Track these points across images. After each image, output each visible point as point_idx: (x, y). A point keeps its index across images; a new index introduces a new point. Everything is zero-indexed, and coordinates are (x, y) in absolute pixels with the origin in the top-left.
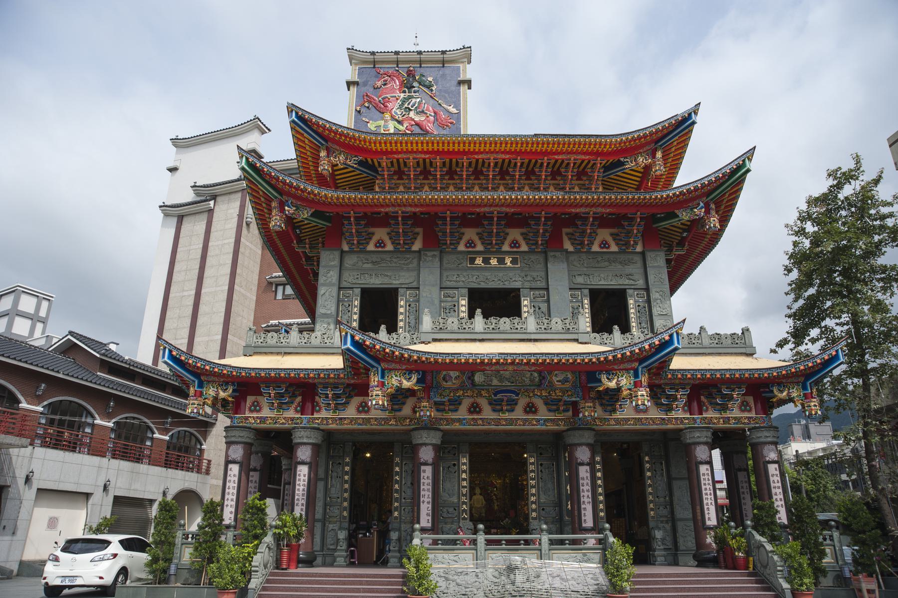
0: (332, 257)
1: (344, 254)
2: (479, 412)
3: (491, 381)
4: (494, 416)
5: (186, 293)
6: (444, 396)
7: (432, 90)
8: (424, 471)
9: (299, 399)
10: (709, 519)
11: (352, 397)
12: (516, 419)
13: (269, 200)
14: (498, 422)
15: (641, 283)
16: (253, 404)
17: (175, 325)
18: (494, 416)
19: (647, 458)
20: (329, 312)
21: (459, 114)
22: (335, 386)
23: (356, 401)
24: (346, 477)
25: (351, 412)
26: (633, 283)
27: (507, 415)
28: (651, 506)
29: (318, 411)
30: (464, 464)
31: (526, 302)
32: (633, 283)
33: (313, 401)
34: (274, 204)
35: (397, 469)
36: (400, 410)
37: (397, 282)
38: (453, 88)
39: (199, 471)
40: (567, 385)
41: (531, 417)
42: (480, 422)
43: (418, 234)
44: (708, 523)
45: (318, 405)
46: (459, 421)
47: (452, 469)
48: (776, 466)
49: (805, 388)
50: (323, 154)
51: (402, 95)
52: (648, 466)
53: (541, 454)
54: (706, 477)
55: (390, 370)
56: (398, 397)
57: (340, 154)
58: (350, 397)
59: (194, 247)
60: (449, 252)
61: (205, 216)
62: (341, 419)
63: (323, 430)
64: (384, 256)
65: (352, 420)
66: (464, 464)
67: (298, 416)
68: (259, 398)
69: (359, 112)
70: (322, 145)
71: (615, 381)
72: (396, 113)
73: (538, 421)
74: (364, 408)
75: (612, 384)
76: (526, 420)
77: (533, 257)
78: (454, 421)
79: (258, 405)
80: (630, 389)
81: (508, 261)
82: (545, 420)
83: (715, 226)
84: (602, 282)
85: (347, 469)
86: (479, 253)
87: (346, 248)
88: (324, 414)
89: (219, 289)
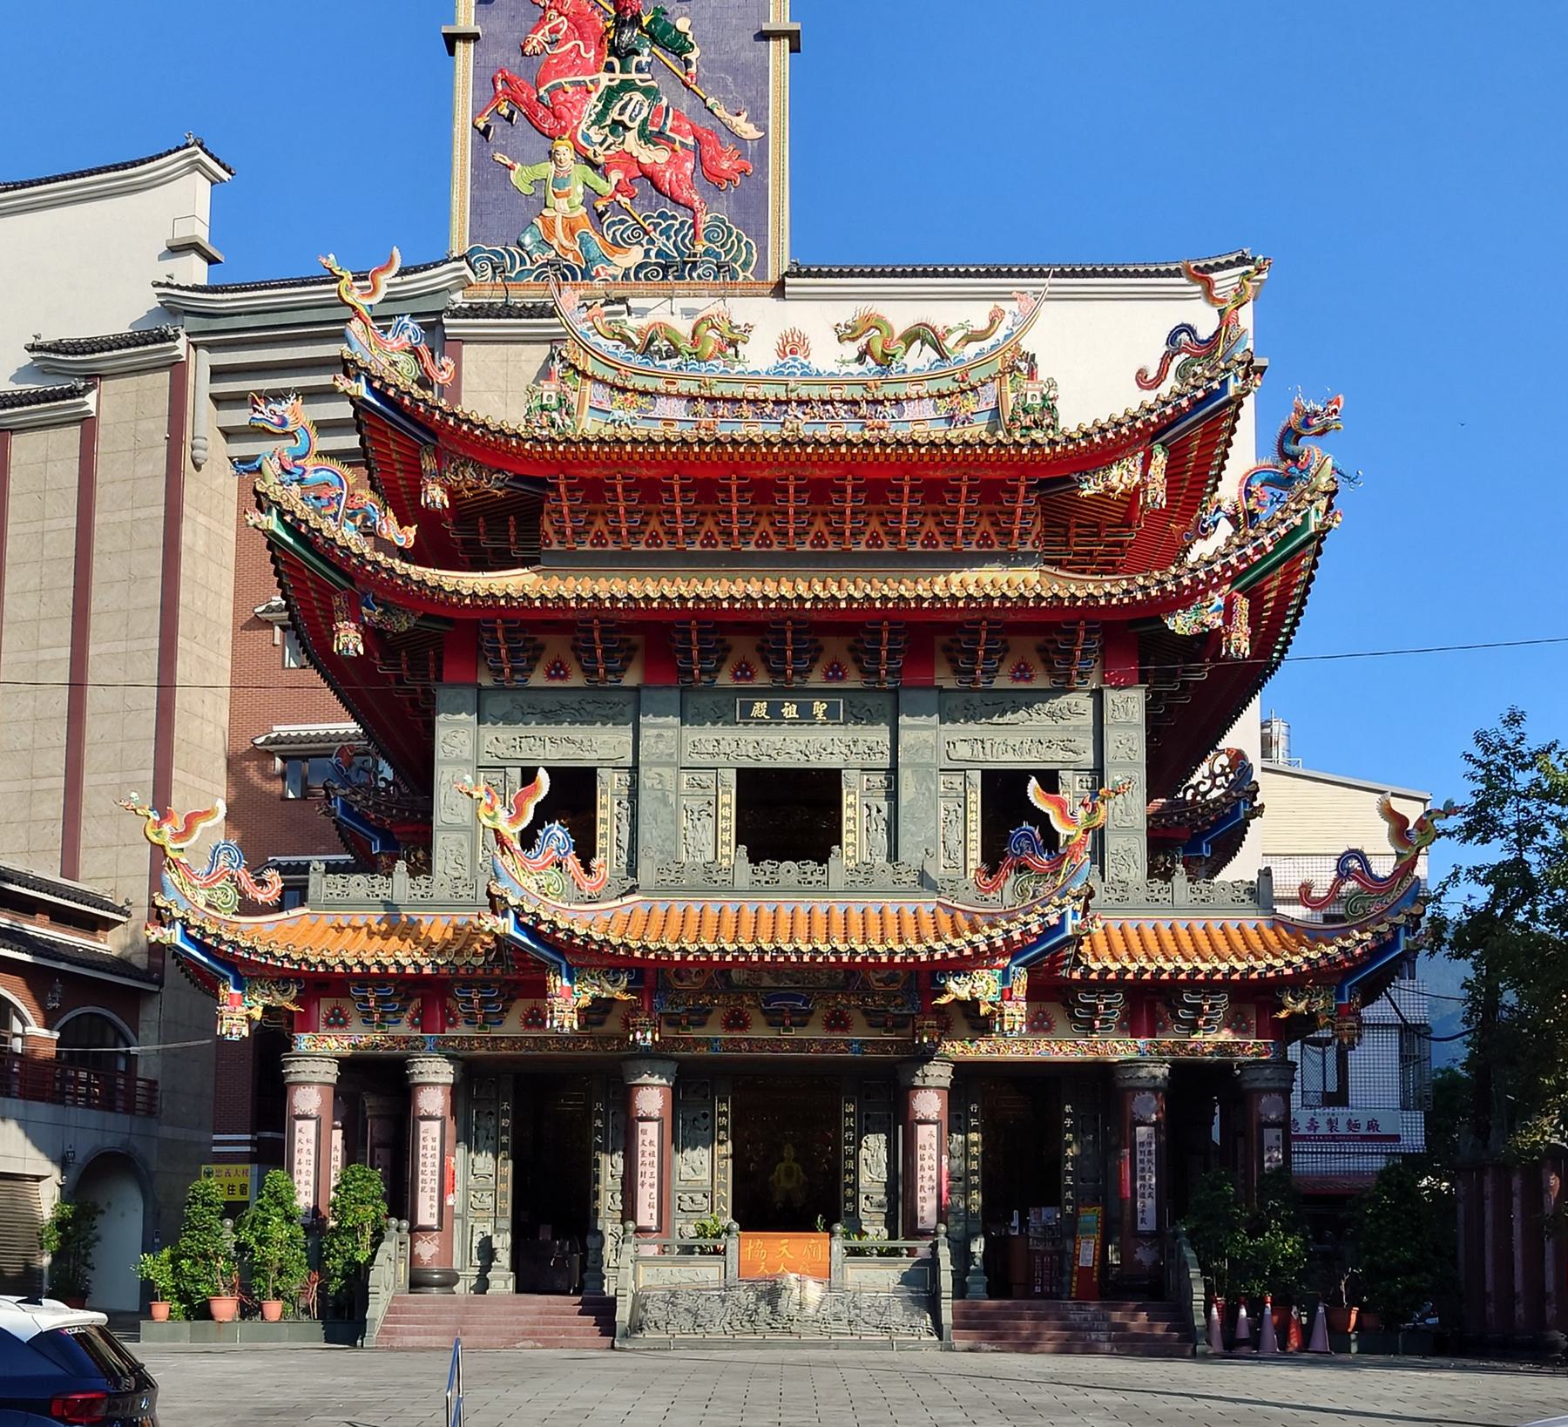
0: (459, 701)
1: (483, 694)
2: (744, 1027)
3: (760, 979)
4: (768, 1034)
5: (46, 655)
6: (678, 1005)
7: (688, 63)
8: (644, 1132)
9: (416, 1003)
10: (1143, 1220)
11: (513, 999)
12: (812, 1037)
13: (326, 592)
14: (776, 1044)
15: (1088, 759)
16: (332, 1014)
17: (27, 740)
18: (768, 1034)
19: (1068, 1108)
20: (458, 820)
21: (763, 141)
22: (484, 984)
23: (520, 1007)
24: (504, 1139)
25: (512, 1026)
26: (1073, 757)
27: (795, 1034)
28: (1069, 1194)
29: (453, 1025)
30: (724, 1114)
31: (851, 799)
32: (1073, 757)
33: (443, 1006)
34: (337, 601)
35: (599, 1123)
36: (601, 1023)
37: (594, 756)
38: (748, 55)
39: (129, 1109)
40: (894, 987)
41: (837, 1036)
42: (745, 1045)
43: (634, 648)
44: (1141, 1227)
45: (451, 1014)
46: (708, 1042)
47: (702, 1123)
48: (1279, 1132)
49: (1340, 996)
50: (428, 463)
51: (604, 79)
52: (1069, 1122)
53: (867, 1097)
54: (1146, 1149)
55: (582, 967)
56: (595, 1013)
57: (464, 465)
58: (512, 999)
59: (54, 524)
60: (700, 690)
61: (75, 431)
62: (494, 1039)
63: (461, 1059)
64: (566, 699)
65: (514, 1041)
66: (724, 1114)
67: (417, 1033)
68: (343, 1002)
69: (485, 133)
70: (426, 443)
71: (968, 987)
72: (587, 138)
73: (848, 1043)
74: (536, 1018)
75: (964, 994)
76: (827, 1043)
77: (871, 701)
78: (697, 1042)
79: (341, 1014)
80: (992, 1003)
81: (819, 708)
82: (862, 1043)
83: (1238, 650)
84: (1009, 757)
85: (505, 1122)
86: (760, 693)
87: (486, 681)
88: (463, 1030)
89: (135, 645)
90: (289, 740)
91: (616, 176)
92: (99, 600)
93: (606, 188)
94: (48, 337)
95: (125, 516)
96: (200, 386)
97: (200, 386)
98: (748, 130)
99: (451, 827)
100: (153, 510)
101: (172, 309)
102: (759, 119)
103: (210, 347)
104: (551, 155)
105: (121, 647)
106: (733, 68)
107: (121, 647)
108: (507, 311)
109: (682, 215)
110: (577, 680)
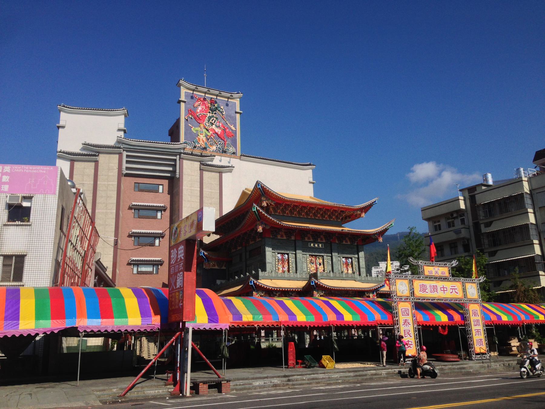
38: (233, 115)
61: (93, 164)
89: (108, 211)
90: (136, 233)
91: (211, 132)
92: (98, 200)
93: (209, 134)
94: (87, 142)
95: (106, 183)
96: (125, 159)
97: (125, 159)
98: (233, 128)
99: (269, 263)
100: (113, 183)
101: (118, 142)
102: (235, 126)
103: (127, 151)
104: (200, 126)
105: (105, 211)
106: (230, 117)
107: (105, 211)
108: (192, 154)
109: (222, 142)
110: (285, 238)
